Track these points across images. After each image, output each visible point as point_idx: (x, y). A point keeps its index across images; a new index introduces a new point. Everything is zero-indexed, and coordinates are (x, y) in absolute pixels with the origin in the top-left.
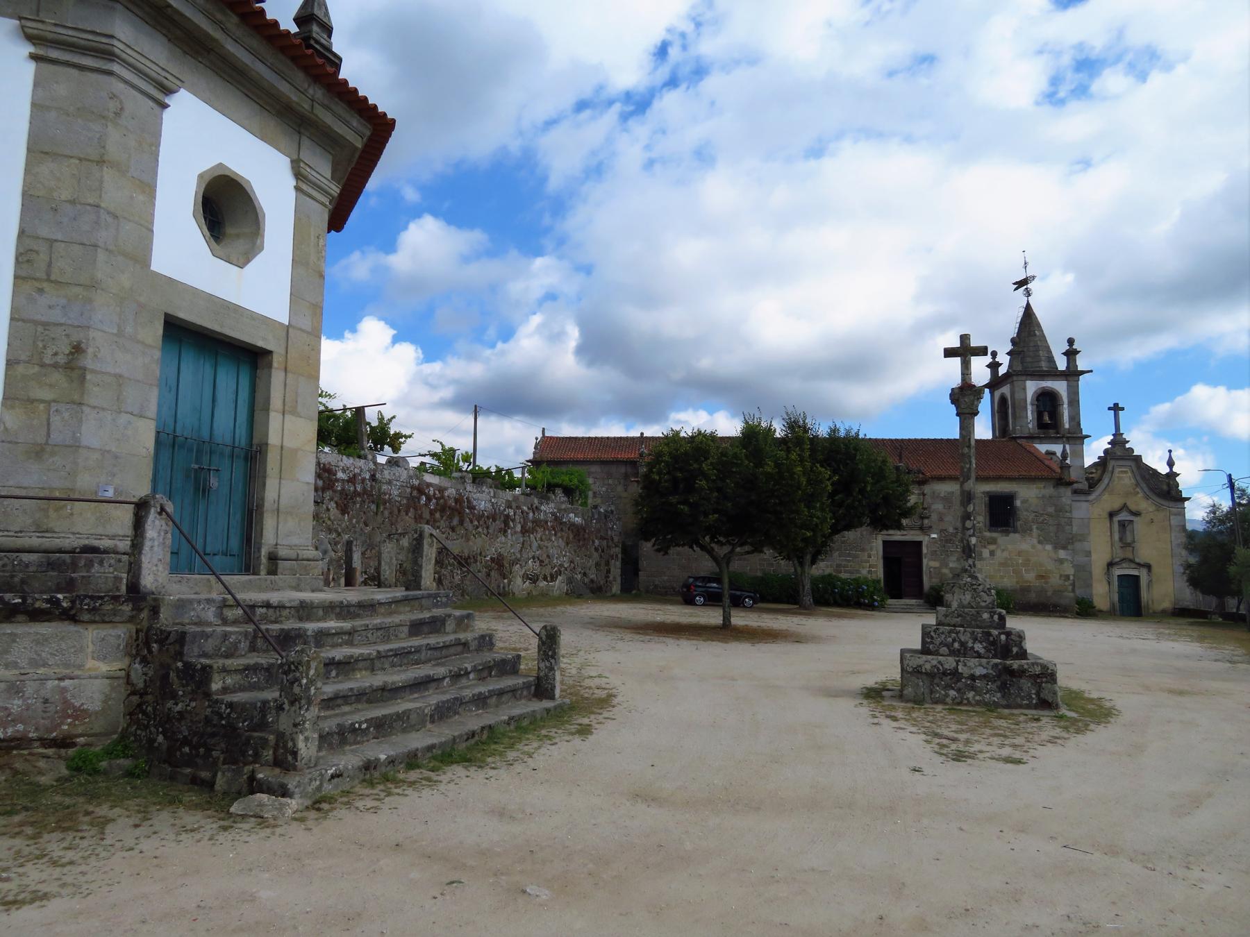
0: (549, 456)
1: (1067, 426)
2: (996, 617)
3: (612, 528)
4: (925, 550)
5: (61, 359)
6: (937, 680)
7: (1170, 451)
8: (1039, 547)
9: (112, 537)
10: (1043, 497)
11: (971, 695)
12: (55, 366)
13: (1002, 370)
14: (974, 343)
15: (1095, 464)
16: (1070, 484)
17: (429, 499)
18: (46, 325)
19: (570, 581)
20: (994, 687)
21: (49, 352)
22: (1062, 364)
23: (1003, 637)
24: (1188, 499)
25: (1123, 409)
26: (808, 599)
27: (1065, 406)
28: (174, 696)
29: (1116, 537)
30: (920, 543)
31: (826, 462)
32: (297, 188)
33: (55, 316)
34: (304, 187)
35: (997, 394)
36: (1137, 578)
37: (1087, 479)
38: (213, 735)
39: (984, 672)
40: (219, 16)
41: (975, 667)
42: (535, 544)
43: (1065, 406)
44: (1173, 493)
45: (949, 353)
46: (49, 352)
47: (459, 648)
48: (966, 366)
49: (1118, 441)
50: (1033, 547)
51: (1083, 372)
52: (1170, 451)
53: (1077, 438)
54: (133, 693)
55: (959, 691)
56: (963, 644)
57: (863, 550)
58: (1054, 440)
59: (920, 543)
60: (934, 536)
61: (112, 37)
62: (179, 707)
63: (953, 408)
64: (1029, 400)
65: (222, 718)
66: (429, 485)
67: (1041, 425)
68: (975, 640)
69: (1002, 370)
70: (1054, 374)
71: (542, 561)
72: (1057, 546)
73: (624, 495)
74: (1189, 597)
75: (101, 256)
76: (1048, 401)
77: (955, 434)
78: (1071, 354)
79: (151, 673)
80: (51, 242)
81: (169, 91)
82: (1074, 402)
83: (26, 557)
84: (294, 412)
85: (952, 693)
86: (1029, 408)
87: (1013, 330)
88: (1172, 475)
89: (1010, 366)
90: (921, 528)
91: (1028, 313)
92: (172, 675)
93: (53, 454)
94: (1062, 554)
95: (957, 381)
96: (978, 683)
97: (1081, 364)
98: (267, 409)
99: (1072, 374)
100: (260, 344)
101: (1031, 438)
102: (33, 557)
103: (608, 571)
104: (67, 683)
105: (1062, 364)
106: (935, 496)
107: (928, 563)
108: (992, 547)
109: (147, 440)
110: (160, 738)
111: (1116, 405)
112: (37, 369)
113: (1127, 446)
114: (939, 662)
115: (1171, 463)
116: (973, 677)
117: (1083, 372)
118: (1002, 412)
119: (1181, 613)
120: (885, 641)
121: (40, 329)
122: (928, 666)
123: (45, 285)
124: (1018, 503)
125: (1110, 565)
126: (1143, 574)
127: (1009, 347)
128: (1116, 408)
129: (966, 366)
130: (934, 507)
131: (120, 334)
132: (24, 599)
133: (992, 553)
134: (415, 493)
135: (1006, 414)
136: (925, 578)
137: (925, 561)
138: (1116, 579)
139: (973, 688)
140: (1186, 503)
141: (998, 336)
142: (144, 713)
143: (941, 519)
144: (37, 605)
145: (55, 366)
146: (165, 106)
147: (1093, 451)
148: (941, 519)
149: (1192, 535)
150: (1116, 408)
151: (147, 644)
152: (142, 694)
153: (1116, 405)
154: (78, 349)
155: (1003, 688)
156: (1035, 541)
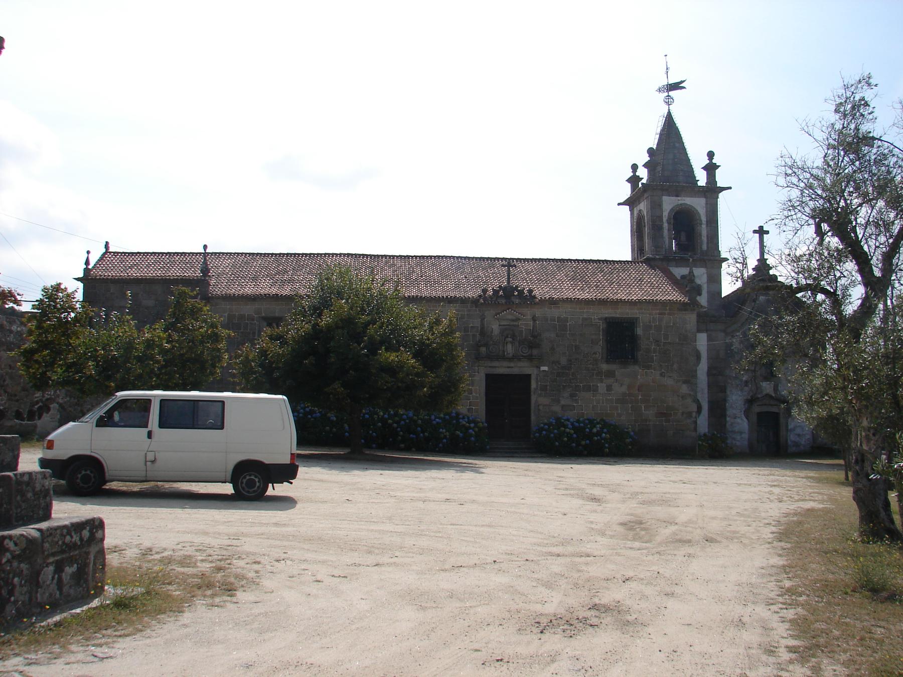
1: (705, 247)
4: (533, 385)
7: (88, 252)
24: (78, 279)
25: (767, 232)
27: (704, 226)
30: (529, 377)
40: (704, 230)
43: (704, 226)
45: (755, 232)
52: (88, 252)
53: (714, 260)
59: (529, 377)
60: (546, 368)
64: (665, 214)
78: (711, 168)
90: (530, 358)
91: (670, 132)
99: (712, 191)
105: (702, 179)
107: (538, 400)
108: (610, 381)
111: (761, 227)
113: (771, 272)
124: (639, 331)
133: (609, 388)
136: (533, 418)
137: (533, 398)
153: (761, 227)
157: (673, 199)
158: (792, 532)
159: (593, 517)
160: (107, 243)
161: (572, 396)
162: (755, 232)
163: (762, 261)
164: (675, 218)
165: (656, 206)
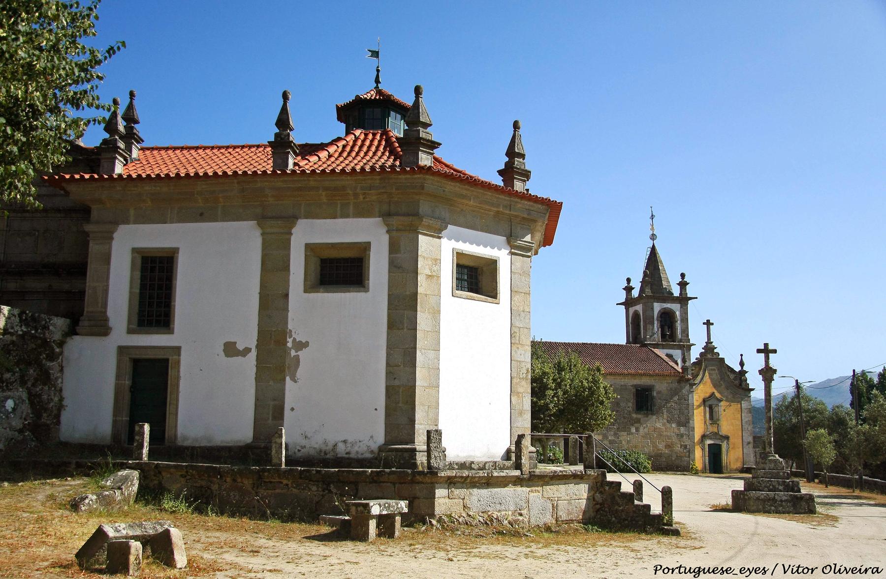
8: (668, 425)
13: (635, 293)
22: (676, 292)
24: (753, 390)
25: (712, 324)
28: (618, 504)
44: (744, 386)
45: (759, 351)
49: (709, 348)
50: (664, 425)
51: (691, 298)
53: (686, 348)
64: (655, 317)
67: (663, 336)
70: (667, 296)
72: (680, 424)
76: (667, 318)
78: (683, 285)
82: (685, 320)
86: (656, 322)
88: (743, 373)
91: (653, 249)
92: (617, 498)
94: (682, 429)
97: (690, 291)
99: (684, 300)
101: (656, 346)
105: (676, 292)
111: (708, 321)
113: (715, 351)
115: (742, 364)
116: (781, 501)
117: (691, 298)
124: (655, 394)
125: (704, 437)
128: (708, 323)
133: (637, 430)
138: (707, 447)
139: (781, 506)
147: (695, 354)
152: (601, 504)
153: (708, 321)
155: (794, 506)
156: (665, 421)
157: (426, 125)
158: (727, 504)
161: (615, 434)
163: (709, 342)
165: (649, 309)
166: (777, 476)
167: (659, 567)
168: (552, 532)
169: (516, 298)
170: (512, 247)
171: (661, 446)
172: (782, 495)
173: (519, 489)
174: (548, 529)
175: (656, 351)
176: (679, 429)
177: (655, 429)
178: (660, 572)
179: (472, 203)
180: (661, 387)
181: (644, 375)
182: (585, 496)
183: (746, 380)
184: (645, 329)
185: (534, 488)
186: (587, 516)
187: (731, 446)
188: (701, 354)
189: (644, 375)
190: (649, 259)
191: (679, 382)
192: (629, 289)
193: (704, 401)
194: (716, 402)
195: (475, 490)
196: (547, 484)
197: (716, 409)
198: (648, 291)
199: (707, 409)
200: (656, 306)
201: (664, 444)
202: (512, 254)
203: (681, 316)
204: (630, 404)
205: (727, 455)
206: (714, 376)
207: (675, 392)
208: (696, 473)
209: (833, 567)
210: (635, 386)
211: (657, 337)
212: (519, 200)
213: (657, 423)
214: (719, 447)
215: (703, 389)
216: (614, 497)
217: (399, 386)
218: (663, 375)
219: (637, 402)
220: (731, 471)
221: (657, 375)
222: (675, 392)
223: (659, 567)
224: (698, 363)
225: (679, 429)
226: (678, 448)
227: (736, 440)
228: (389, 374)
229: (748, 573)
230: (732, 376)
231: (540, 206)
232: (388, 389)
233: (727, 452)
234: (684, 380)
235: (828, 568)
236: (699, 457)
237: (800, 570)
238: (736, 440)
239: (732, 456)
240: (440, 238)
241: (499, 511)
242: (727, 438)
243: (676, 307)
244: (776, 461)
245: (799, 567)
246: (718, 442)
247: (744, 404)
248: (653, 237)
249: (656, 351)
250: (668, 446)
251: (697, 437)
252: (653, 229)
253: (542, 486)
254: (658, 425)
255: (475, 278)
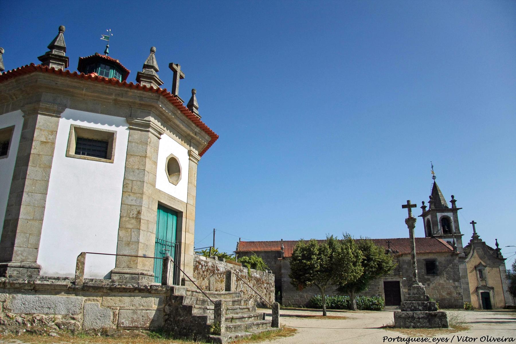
0: (242, 249)
1: (454, 231)
2: (426, 297)
3: (271, 279)
4: (401, 285)
5: (135, 216)
6: (407, 320)
8: (448, 281)
9: (146, 271)
10: (447, 260)
11: (418, 324)
12: (133, 218)
13: (427, 209)
14: (412, 203)
15: (467, 246)
16: (457, 254)
17: (202, 266)
18: (131, 205)
19: (256, 301)
20: (426, 321)
21: (131, 214)
22: (450, 206)
23: (428, 304)
24: (506, 259)
25: (476, 223)
26: (355, 306)
28: (180, 315)
29: (479, 276)
30: (399, 282)
31: (360, 248)
32: (189, 159)
33: (133, 203)
34: (191, 158)
35: (426, 219)
36: (488, 293)
37: (464, 252)
38: (193, 326)
39: (423, 316)
41: (420, 314)
42: (241, 286)
45: (404, 207)
46: (131, 214)
47: (247, 310)
48: (410, 211)
49: (475, 237)
50: (445, 281)
53: (459, 237)
54: (166, 315)
55: (414, 323)
56: (415, 307)
57: (376, 286)
58: (450, 237)
59: (399, 282)
61: (150, 121)
62: (182, 319)
63: (407, 226)
64: (438, 221)
65: (196, 321)
66: (202, 261)
67: (445, 232)
68: (419, 305)
69: (427, 209)
70: (445, 209)
71: (244, 293)
72: (455, 280)
73: (275, 265)
74: (510, 301)
75: (145, 184)
76: (446, 221)
77: (408, 236)
78: (453, 202)
79: (172, 309)
80: (132, 181)
81: (160, 134)
82: (456, 221)
83: (126, 276)
84: (188, 232)
85: (412, 324)
86: (439, 224)
87: (430, 193)
88: (498, 250)
89: (430, 207)
92: (179, 310)
93: (132, 244)
94: (457, 284)
95: (407, 216)
96: (421, 320)
97: (458, 205)
98: (181, 231)
99: (455, 210)
100: (180, 209)
101: (441, 237)
102: (128, 275)
103: (270, 297)
104: (148, 311)
105: (450, 206)
106: (404, 262)
108: (428, 282)
109: (154, 240)
110: (176, 328)
111: (473, 221)
112: (128, 219)
113: (479, 238)
114: (407, 314)
115: (497, 245)
116: (419, 318)
118: (428, 226)
119: (507, 308)
120: (388, 316)
121: (129, 207)
122: (404, 315)
123: (130, 194)
124: (437, 263)
125: (477, 288)
126: (491, 293)
127: (429, 200)
128: (473, 223)
129: (410, 211)
130: (404, 266)
131: (148, 208)
132: (138, 285)
134: (197, 264)
135: (430, 227)
137: (401, 290)
138: (480, 294)
139: (419, 322)
140: (505, 261)
141: (424, 197)
142: (170, 321)
143: (407, 272)
144: (142, 287)
145: (133, 218)
146: (159, 138)
147: (466, 241)
148: (407, 272)
149: (508, 276)
150: (473, 223)
151: (170, 300)
152: (169, 315)
153: (473, 221)
154: (139, 213)
155: (429, 321)
156: (445, 279)
159: (202, 146)
160: (193, 90)
162: (404, 207)
163: (475, 233)
164: (442, 221)
166: (419, 299)
167: (386, 338)
168: (107, 335)
169: (131, 160)
170: (131, 124)
171: (444, 294)
172: (420, 314)
173: (73, 297)
174: (105, 333)
175: (441, 240)
176: (454, 284)
177: (439, 284)
178: (386, 341)
179: (84, 92)
180: (441, 259)
181: (430, 253)
182: (155, 307)
183: (501, 254)
184: (433, 229)
185: (92, 298)
186: (156, 324)
187: (496, 293)
188: (471, 241)
189: (430, 253)
190: (433, 190)
191: (452, 256)
192: (424, 207)
193: (475, 267)
194: (483, 268)
195: (20, 295)
196: (108, 295)
197: (484, 272)
198: (433, 207)
199: (478, 272)
200: (440, 215)
201: (446, 292)
202: (130, 129)
203: (454, 219)
204: (423, 271)
205: (494, 299)
206: (480, 253)
207: (450, 262)
208: (473, 309)
209: (486, 337)
210: (425, 260)
211: (441, 232)
212: (129, 90)
213: (440, 280)
214: (488, 294)
215: (473, 260)
216: (177, 309)
217: (10, 220)
218: (441, 252)
219: (427, 269)
220: (498, 308)
221: (438, 253)
222: (450, 262)
223: (386, 338)
224: (469, 246)
225: (454, 284)
226: (455, 295)
227: (498, 289)
228: (8, 211)
229: (437, 341)
230: (491, 252)
231: (150, 94)
232: (6, 221)
233: (494, 296)
234: (457, 256)
235: (484, 338)
236: (475, 300)
237: (468, 339)
238: (498, 289)
239: (496, 299)
240: (59, 117)
241: (47, 314)
242: (492, 288)
243: (450, 215)
244: (419, 288)
245: (467, 337)
246: (486, 291)
247: (501, 268)
248: (434, 178)
249: (441, 240)
250: (448, 294)
251: (472, 288)
252: (433, 173)
253: (102, 296)
254: (441, 282)
255: (93, 146)
